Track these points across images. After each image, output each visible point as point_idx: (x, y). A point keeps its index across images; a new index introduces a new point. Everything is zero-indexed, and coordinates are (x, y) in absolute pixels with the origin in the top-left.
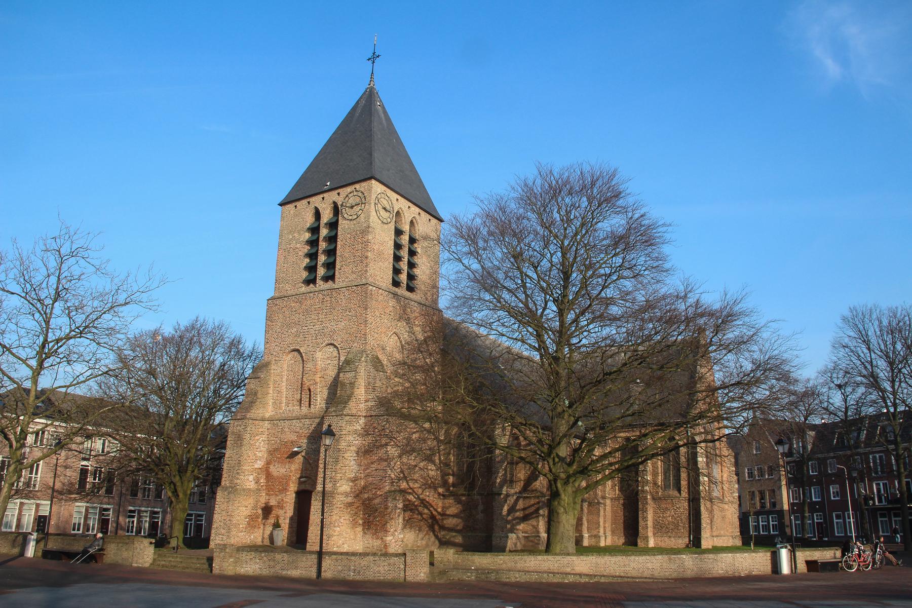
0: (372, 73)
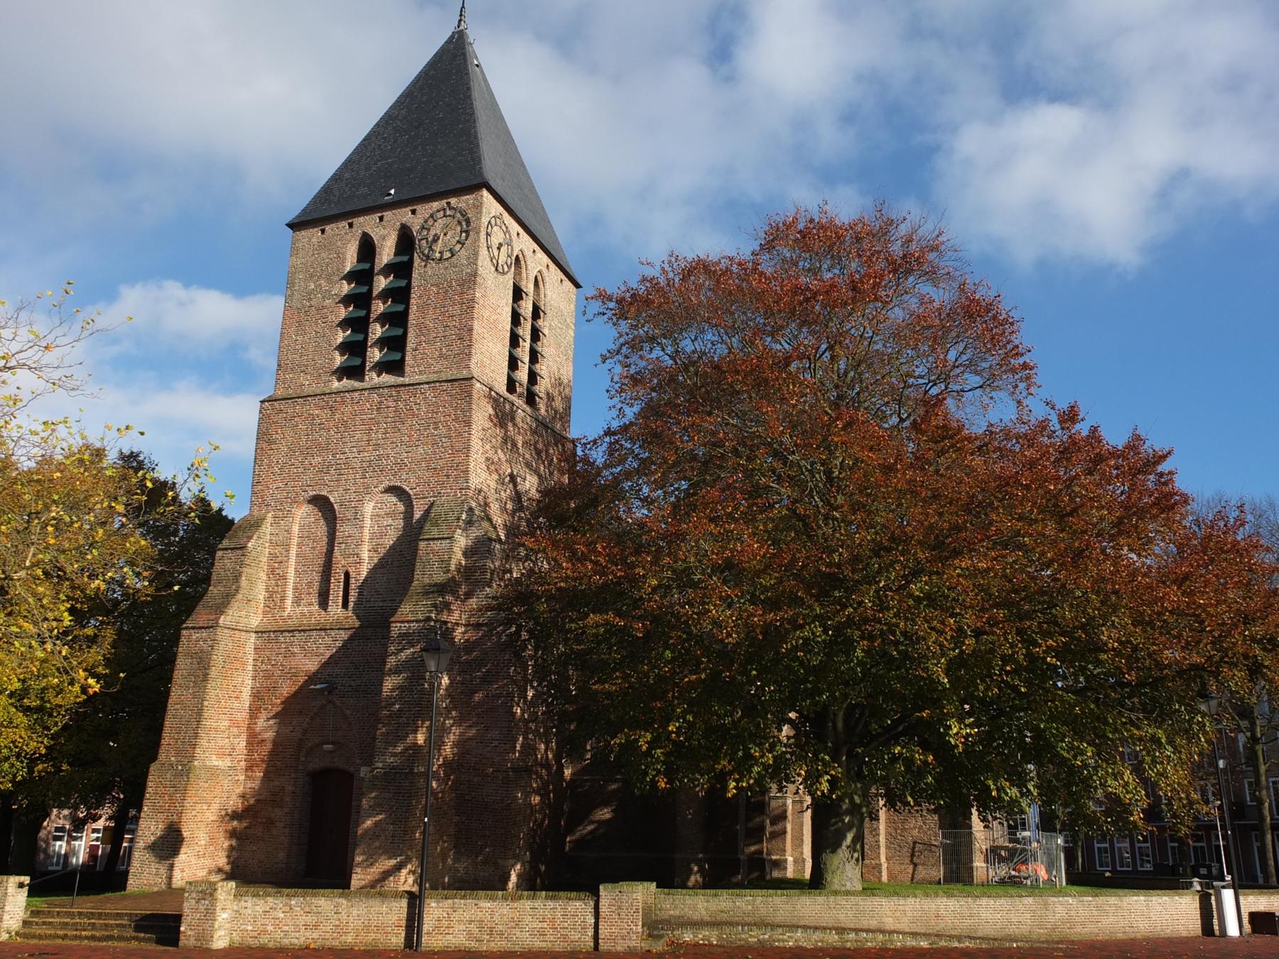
0: (463, 7)
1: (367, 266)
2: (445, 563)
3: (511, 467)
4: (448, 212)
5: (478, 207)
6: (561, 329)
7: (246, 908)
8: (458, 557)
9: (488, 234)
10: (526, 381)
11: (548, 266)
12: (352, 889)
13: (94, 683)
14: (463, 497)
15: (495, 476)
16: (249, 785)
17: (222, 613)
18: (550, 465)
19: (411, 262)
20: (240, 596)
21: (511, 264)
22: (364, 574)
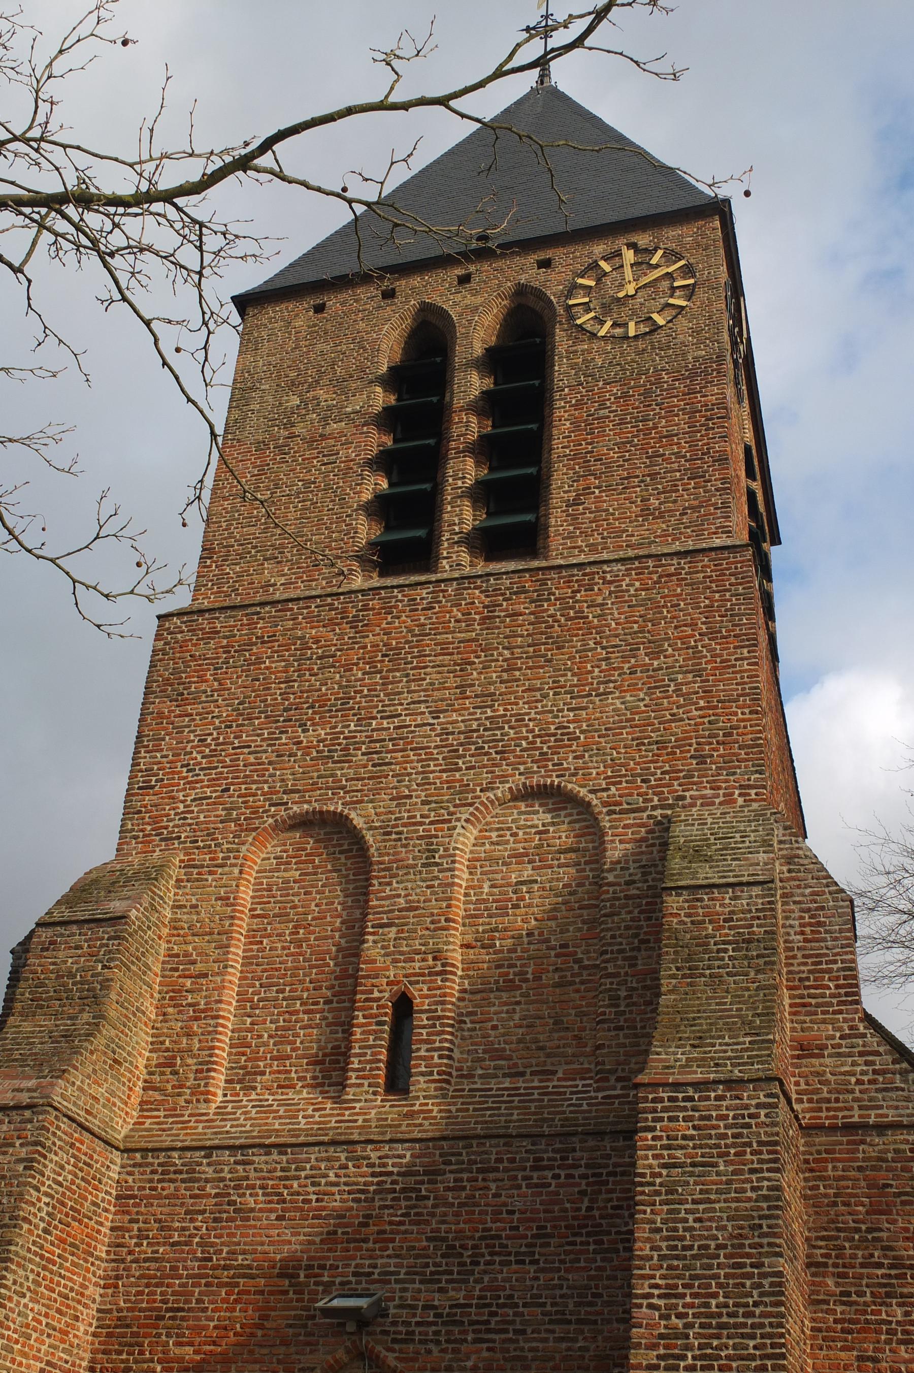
20: (99, 1042)
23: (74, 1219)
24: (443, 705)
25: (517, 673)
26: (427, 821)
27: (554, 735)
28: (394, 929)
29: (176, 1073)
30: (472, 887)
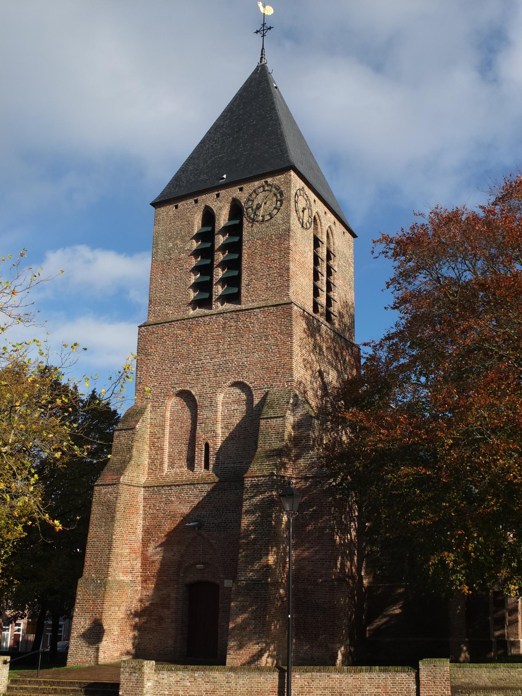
0: (263, 49)
1: (209, 229)
2: (280, 435)
3: (320, 366)
4: (266, 188)
5: (288, 183)
6: (345, 267)
7: (163, 679)
8: (289, 429)
9: (296, 202)
10: (325, 304)
11: (335, 222)
12: (227, 665)
13: (58, 524)
14: (290, 387)
15: (310, 372)
16: (145, 593)
17: (122, 474)
18: (344, 363)
19: (241, 225)
20: (132, 462)
21: (311, 222)
22: (219, 444)
23: (132, 507)
24: (213, 356)
25: (232, 346)
26: (210, 392)
27: (241, 366)
28: (204, 424)
29: (155, 465)
30: (223, 411)
